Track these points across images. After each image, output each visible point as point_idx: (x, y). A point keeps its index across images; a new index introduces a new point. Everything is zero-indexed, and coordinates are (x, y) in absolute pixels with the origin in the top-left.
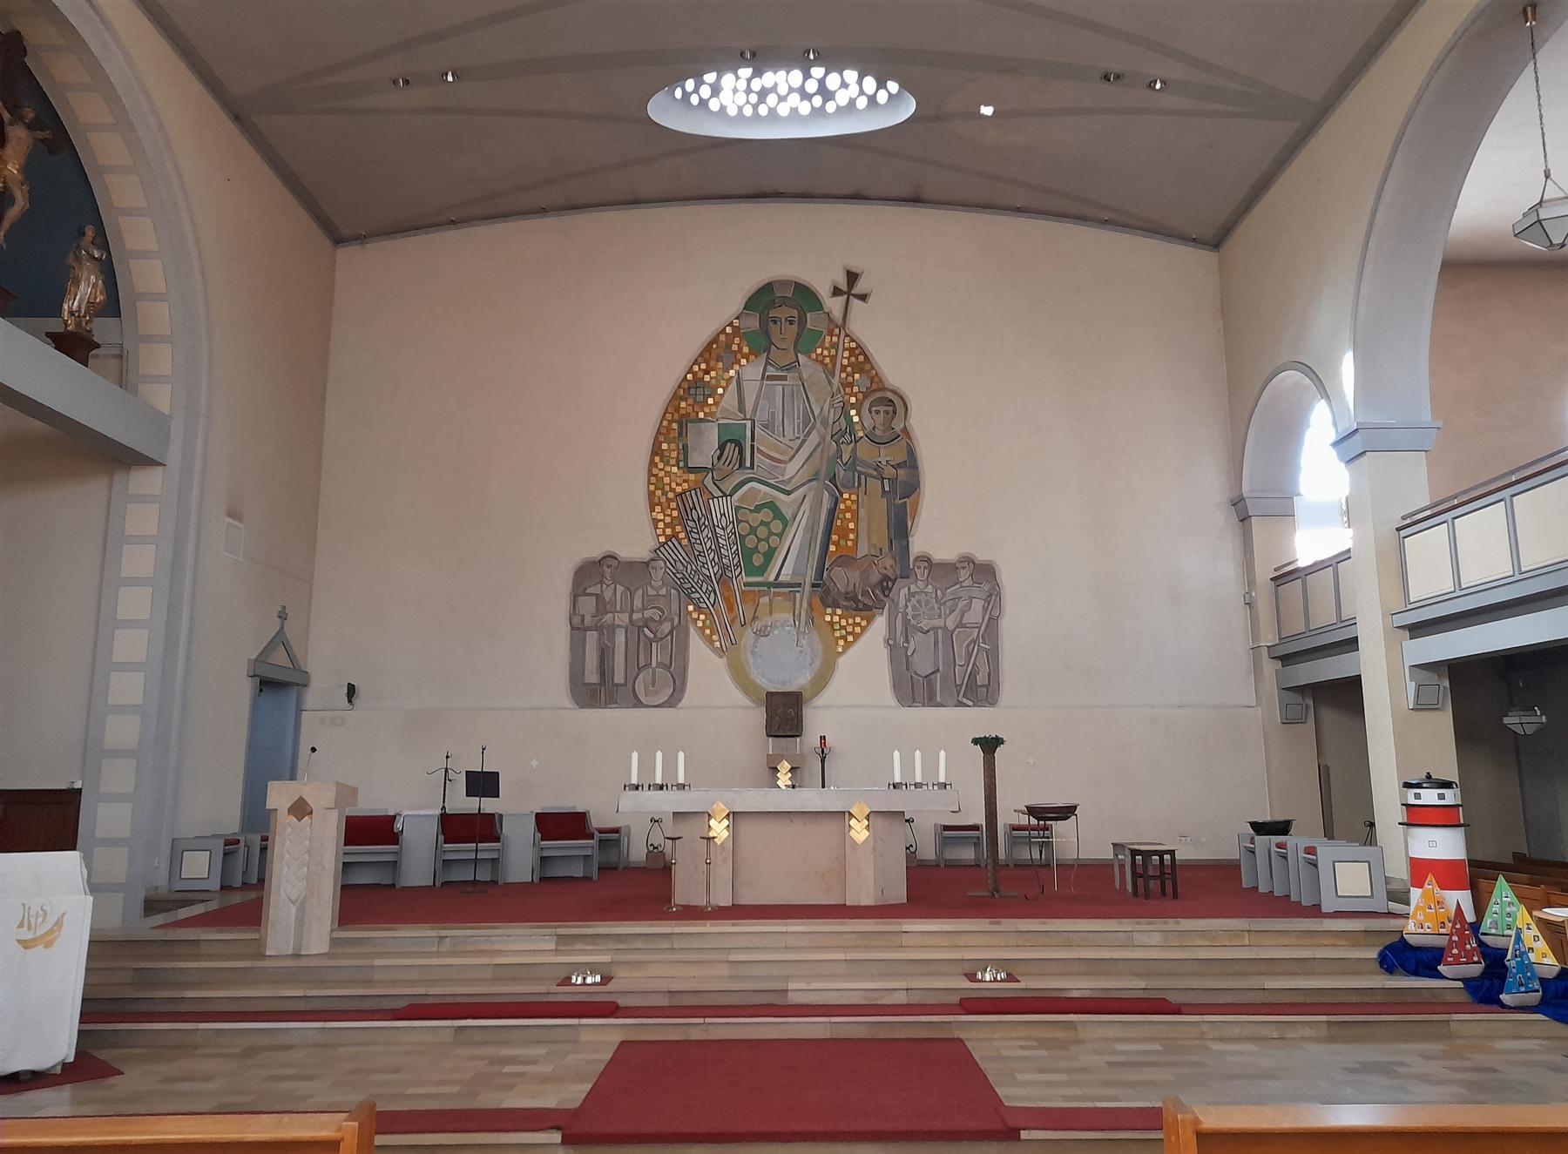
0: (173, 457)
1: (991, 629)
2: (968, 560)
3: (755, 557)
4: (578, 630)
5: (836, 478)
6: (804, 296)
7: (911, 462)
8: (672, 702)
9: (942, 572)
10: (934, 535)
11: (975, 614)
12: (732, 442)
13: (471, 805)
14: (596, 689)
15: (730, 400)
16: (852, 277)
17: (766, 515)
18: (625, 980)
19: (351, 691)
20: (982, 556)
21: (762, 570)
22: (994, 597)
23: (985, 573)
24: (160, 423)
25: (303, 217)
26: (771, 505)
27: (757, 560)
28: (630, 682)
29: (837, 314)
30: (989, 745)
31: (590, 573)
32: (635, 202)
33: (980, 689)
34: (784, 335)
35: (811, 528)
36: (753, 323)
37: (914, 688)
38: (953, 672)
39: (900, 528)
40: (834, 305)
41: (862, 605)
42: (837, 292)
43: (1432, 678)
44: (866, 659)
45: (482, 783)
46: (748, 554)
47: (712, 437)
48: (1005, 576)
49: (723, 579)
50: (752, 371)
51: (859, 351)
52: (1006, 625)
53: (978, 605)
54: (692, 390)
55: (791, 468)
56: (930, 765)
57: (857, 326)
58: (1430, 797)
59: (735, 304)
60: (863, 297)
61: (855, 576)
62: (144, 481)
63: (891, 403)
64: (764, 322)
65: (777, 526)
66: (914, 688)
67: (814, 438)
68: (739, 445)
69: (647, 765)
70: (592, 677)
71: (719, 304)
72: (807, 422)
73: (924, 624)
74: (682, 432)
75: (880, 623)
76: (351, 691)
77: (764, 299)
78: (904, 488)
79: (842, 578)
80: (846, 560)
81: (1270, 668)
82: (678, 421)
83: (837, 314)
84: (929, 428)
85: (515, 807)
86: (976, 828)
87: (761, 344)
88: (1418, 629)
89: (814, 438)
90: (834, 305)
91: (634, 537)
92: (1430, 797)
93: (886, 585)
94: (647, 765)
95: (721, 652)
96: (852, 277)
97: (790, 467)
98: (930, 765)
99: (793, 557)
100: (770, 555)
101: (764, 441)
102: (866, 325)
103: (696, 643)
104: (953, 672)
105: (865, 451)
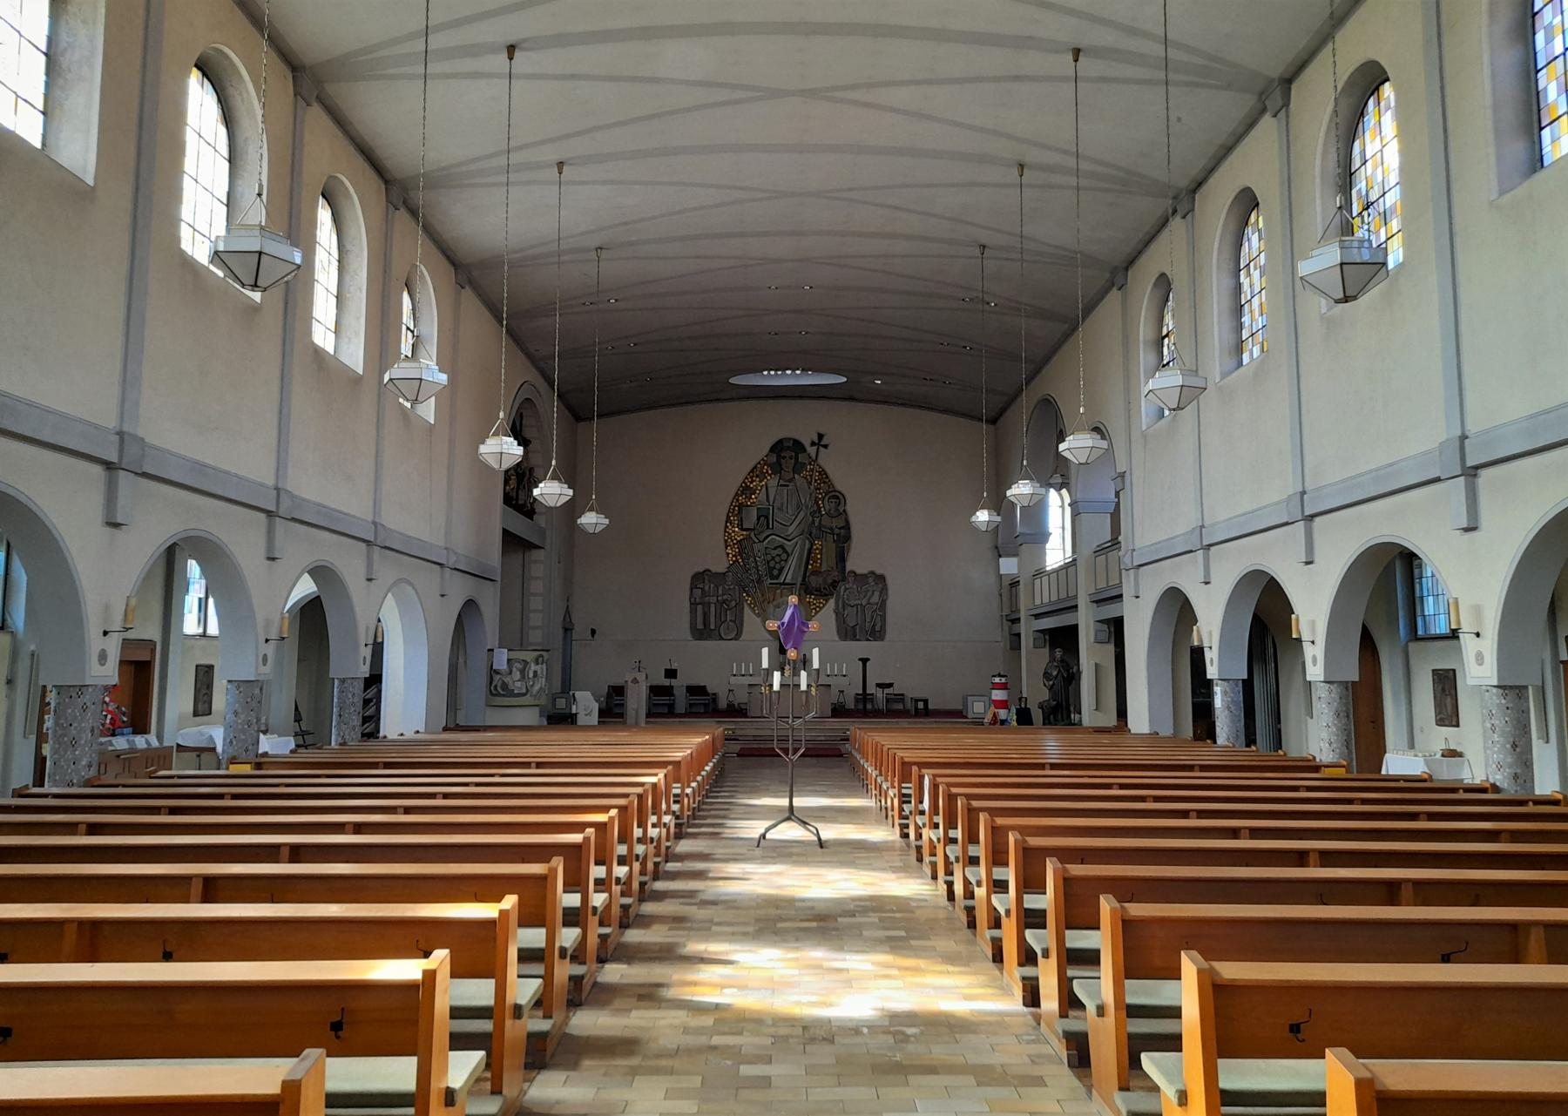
0: (548, 547)
1: (883, 605)
2: (873, 573)
3: (774, 571)
4: (693, 605)
5: (813, 532)
6: (798, 446)
7: (847, 527)
8: (737, 638)
9: (861, 579)
10: (858, 562)
11: (875, 599)
12: (763, 515)
13: (667, 682)
14: (702, 632)
15: (763, 496)
16: (821, 436)
17: (779, 551)
18: (738, 732)
19: (593, 632)
20: (879, 572)
21: (777, 577)
22: (884, 590)
23: (881, 579)
24: (542, 532)
25: (366, 165)
26: (782, 547)
27: (775, 572)
28: (718, 628)
29: (813, 455)
30: (864, 661)
31: (698, 578)
32: (718, 400)
33: (877, 634)
34: (788, 464)
35: (800, 558)
36: (774, 459)
37: (847, 632)
38: (864, 625)
39: (842, 558)
40: (812, 450)
41: (823, 594)
42: (813, 444)
43: (1105, 627)
44: (823, 622)
45: (671, 674)
46: (771, 569)
47: (754, 513)
48: (889, 581)
49: (759, 581)
50: (773, 482)
51: (823, 473)
52: (889, 603)
53: (877, 594)
54: (745, 490)
55: (791, 529)
56: (840, 669)
57: (821, 461)
58: (997, 680)
59: (766, 450)
60: (826, 446)
61: (820, 580)
62: (537, 555)
63: (838, 498)
64: (779, 457)
65: (784, 556)
66: (847, 632)
67: (802, 514)
68: (767, 517)
69: (739, 667)
70: (700, 626)
71: (760, 449)
72: (799, 508)
73: (852, 603)
74: (740, 511)
75: (832, 602)
76: (593, 632)
77: (778, 447)
78: (843, 538)
79: (815, 581)
80: (816, 573)
81: (1007, 624)
82: (737, 510)
83: (813, 455)
84: (852, 508)
85: (679, 684)
86: (1278, 742)
87: (777, 468)
88: (1037, 616)
89: (802, 514)
90: (812, 450)
91: (720, 566)
92: (997, 680)
93: (834, 584)
94: (739, 667)
95: (758, 615)
96: (821, 436)
97: (791, 526)
98: (840, 669)
99: (790, 573)
100: (782, 569)
101: (779, 516)
102: (827, 460)
103: (747, 610)
104: (864, 625)
105: (826, 521)
